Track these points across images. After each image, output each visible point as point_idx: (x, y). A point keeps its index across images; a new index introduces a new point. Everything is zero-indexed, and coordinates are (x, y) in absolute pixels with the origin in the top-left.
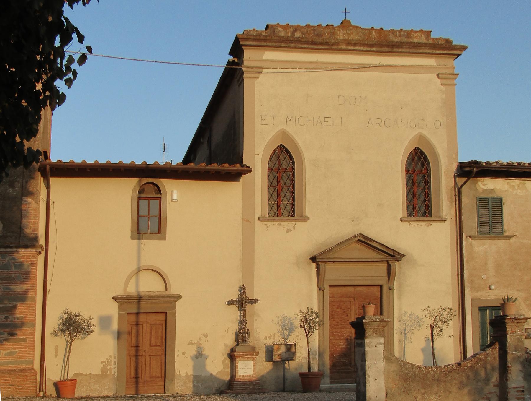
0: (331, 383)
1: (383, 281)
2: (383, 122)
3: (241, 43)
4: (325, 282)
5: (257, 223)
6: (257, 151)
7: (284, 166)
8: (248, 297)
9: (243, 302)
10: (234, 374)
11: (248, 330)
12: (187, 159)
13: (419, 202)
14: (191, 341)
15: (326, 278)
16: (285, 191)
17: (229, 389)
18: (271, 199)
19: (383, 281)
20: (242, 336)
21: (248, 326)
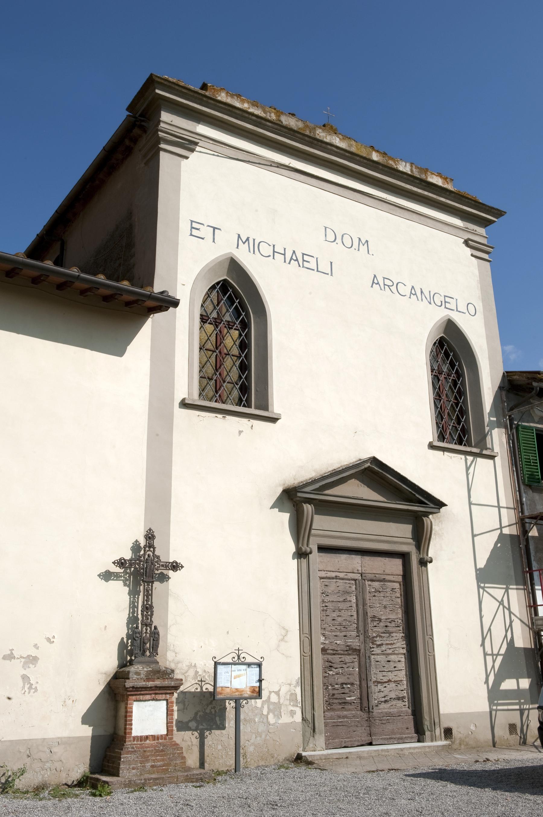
0: (328, 747)
1: (410, 548)
2: (395, 285)
3: (162, 146)
4: (311, 538)
5: (181, 414)
6: (184, 267)
7: (235, 302)
8: (158, 557)
9: (144, 570)
10: (121, 733)
11: (155, 628)
12: (37, 250)
13: (456, 426)
14: (12, 650)
15: (313, 532)
16: (236, 370)
17: (103, 772)
18: (208, 302)
19: (410, 548)
20: (141, 641)
21: (156, 621)
